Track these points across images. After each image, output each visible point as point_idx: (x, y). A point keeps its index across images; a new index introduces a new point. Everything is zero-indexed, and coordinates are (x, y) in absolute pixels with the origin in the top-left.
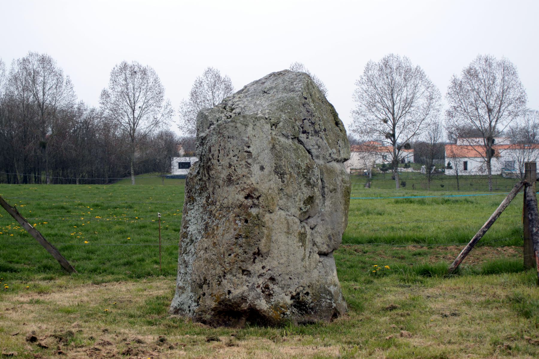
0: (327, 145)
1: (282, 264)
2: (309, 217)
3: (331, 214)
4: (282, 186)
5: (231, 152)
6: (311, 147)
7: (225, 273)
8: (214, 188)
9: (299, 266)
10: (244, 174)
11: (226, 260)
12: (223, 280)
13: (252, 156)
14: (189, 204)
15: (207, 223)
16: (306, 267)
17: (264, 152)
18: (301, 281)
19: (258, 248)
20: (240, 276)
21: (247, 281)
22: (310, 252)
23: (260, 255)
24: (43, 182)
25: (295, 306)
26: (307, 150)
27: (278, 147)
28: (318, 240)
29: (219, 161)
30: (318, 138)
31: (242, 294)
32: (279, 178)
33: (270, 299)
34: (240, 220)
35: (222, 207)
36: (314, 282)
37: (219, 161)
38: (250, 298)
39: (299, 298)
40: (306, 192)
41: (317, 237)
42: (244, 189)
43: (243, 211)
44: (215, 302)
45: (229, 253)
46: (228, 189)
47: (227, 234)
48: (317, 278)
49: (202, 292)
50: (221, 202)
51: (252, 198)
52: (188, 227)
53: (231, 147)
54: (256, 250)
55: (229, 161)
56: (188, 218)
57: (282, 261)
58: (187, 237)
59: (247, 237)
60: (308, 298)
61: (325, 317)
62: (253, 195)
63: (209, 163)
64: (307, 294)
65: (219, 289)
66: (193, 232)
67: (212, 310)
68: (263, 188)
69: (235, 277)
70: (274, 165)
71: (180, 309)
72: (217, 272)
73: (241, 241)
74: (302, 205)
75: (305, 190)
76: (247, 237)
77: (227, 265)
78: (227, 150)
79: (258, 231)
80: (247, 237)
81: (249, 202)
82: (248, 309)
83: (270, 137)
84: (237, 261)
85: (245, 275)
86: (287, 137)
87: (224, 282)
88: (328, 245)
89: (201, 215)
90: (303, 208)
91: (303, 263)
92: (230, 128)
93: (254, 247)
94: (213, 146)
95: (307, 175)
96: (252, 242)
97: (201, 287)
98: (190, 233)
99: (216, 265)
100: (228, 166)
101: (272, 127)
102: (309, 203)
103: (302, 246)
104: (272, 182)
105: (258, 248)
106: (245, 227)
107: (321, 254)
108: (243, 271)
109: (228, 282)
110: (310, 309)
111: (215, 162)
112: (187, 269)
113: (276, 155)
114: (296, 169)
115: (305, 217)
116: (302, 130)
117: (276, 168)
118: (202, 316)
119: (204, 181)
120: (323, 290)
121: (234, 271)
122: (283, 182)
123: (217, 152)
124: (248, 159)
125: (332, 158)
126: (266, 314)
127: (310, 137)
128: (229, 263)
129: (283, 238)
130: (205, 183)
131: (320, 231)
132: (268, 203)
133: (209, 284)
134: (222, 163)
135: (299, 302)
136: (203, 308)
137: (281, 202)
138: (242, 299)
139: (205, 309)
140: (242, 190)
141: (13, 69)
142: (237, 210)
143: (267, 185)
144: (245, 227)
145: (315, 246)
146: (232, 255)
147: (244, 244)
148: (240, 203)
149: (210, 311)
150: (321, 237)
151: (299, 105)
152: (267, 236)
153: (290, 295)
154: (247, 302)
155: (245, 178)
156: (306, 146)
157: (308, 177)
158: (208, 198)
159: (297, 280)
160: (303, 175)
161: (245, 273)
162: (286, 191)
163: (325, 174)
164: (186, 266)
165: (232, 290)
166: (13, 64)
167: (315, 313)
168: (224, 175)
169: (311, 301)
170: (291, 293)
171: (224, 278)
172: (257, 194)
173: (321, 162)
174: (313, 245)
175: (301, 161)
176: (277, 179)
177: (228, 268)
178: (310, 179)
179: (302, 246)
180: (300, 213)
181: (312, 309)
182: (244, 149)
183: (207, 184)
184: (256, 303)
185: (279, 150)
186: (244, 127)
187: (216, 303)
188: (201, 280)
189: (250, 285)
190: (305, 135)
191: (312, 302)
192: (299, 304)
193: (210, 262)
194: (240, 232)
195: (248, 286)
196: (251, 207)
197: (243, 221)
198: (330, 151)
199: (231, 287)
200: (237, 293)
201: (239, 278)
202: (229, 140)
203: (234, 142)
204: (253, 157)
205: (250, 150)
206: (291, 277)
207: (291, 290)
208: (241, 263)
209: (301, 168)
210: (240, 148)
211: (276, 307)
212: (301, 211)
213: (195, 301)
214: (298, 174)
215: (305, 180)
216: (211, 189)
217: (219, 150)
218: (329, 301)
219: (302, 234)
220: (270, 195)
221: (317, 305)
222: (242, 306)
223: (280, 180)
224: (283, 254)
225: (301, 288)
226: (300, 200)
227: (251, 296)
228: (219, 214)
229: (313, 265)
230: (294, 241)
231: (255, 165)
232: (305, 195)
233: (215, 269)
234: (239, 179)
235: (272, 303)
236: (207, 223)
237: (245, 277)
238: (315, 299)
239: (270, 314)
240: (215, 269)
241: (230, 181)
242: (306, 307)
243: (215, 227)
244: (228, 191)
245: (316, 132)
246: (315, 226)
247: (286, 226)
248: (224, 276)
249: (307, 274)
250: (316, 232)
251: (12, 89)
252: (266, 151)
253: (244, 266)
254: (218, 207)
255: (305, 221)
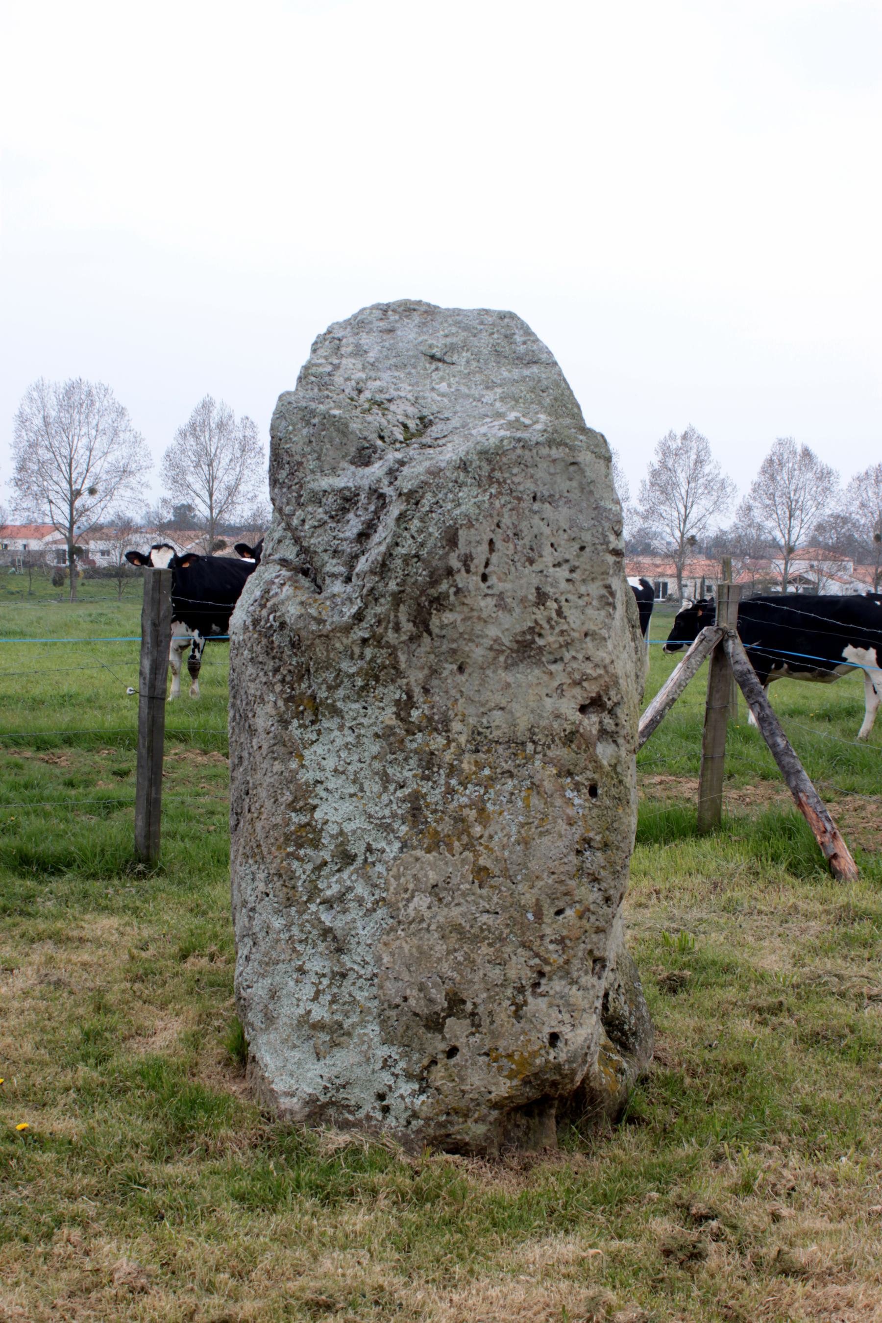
5: (547, 550)
7: (541, 974)
8: (434, 672)
10: (591, 626)
11: (548, 931)
12: (530, 999)
14: (295, 723)
15: (415, 798)
24: (821, 754)
29: (484, 578)
34: (577, 787)
35: (479, 741)
37: (484, 578)
42: (586, 678)
44: (510, 1077)
45: (561, 904)
46: (511, 679)
47: (546, 840)
49: (443, 1046)
50: (472, 721)
52: (315, 807)
53: (547, 531)
55: (535, 581)
56: (306, 776)
58: (316, 844)
59: (606, 845)
63: (444, 586)
65: (524, 1032)
66: (348, 827)
67: (495, 1106)
69: (575, 988)
71: (331, 1103)
72: (512, 974)
76: (606, 846)
77: (552, 947)
78: (526, 541)
81: (591, 723)
87: (536, 1005)
89: (377, 765)
92: (543, 465)
94: (470, 525)
97: (435, 1024)
98: (333, 829)
99: (508, 949)
100: (532, 597)
106: (595, 810)
109: (550, 1005)
111: (470, 581)
112: (345, 958)
118: (452, 1130)
119: (388, 645)
123: (485, 547)
128: (561, 941)
130: (393, 654)
133: (473, 1014)
134: (500, 586)
136: (452, 1101)
139: (463, 1104)
140: (577, 683)
142: (557, 752)
146: (569, 912)
148: (569, 728)
149: (484, 1110)
155: (589, 643)
158: (405, 705)
164: (339, 950)
165: (565, 1031)
168: (504, 627)
171: (534, 993)
177: (557, 959)
182: (608, 543)
183: (402, 658)
187: (516, 1082)
188: (431, 1001)
193: (476, 940)
199: (562, 1022)
201: (586, 989)
202: (536, 506)
203: (562, 514)
208: (595, 938)
210: (587, 537)
213: (409, 1076)
216: (415, 677)
217: (491, 542)
228: (480, 766)
233: (503, 963)
234: (567, 645)
236: (415, 798)
240: (503, 963)
241: (526, 649)
243: (472, 814)
244: (508, 685)
248: (536, 985)
254: (463, 739)
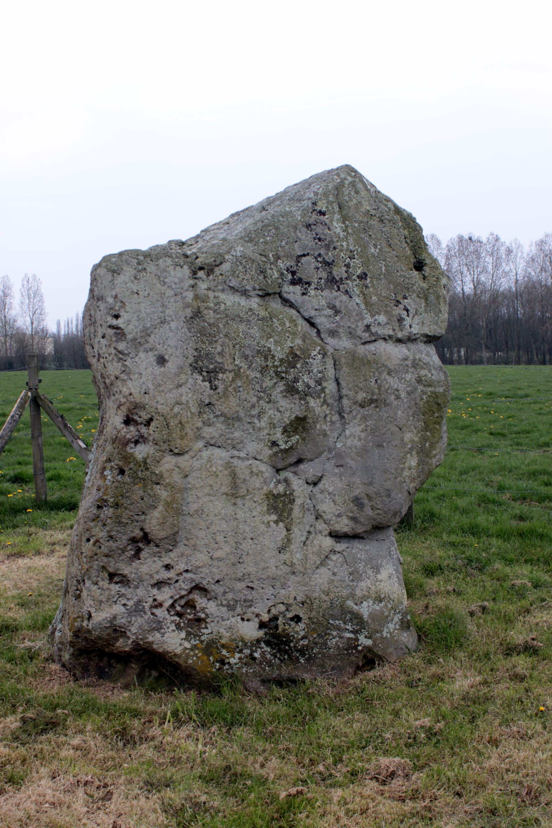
0: (363, 306)
1: (219, 559)
2: (300, 461)
3: (363, 452)
4: (210, 396)
6: (313, 313)
9: (272, 563)
13: (124, 335)
16: (292, 565)
17: (166, 326)
18: (283, 591)
19: (142, 529)
20: (105, 584)
21: (121, 596)
22: (309, 532)
23: (152, 544)
25: (268, 643)
26: (305, 319)
27: (210, 316)
28: (327, 507)
30: (335, 294)
31: (110, 622)
32: (204, 381)
33: (199, 629)
36: (316, 595)
38: (134, 629)
39: (277, 627)
40: (289, 409)
41: (322, 501)
43: (116, 451)
48: (325, 587)
51: (136, 423)
54: (138, 533)
57: (218, 554)
60: (297, 629)
61: (333, 669)
62: (136, 417)
64: (297, 619)
68: (161, 402)
70: (191, 352)
73: (108, 512)
74: (278, 436)
75: (284, 403)
76: (117, 505)
79: (141, 493)
80: (117, 505)
81: (131, 432)
82: (134, 649)
83: (190, 295)
84: (96, 554)
85: (117, 583)
86: (245, 293)
88: (354, 519)
90: (280, 443)
91: (285, 557)
93: (130, 528)
95: (286, 372)
96: (125, 515)
101: (195, 273)
102: (296, 431)
103: (276, 522)
104: (183, 390)
105: (142, 529)
107: (336, 536)
108: (112, 576)
110: (298, 651)
113: (202, 332)
114: (259, 361)
115: (287, 460)
116: (290, 277)
117: (197, 359)
120: (336, 612)
121: (94, 573)
122: (214, 388)
124: (117, 341)
125: (372, 334)
126: (181, 662)
127: (312, 292)
129: (219, 506)
131: (331, 490)
132: (170, 434)
135: (276, 636)
137: (208, 432)
138: (115, 630)
141: (531, 251)
143: (171, 397)
144: (116, 484)
145: (320, 521)
147: (109, 521)
150: (334, 502)
151: (295, 228)
152: (168, 505)
153: (257, 620)
154: (129, 638)
156: (301, 310)
157: (291, 377)
159: (272, 591)
160: (277, 373)
161: (116, 579)
162: (220, 407)
163: (345, 369)
166: (530, 246)
167: (308, 660)
169: (302, 633)
170: (257, 615)
172: (145, 416)
173: (344, 343)
174: (317, 518)
175: (276, 342)
176: (199, 382)
178: (296, 380)
179: (276, 522)
180: (270, 452)
181: (302, 652)
184: (150, 639)
185: (212, 321)
186: (109, 276)
189: (130, 603)
190: (298, 289)
191: (304, 638)
192: (275, 636)
194: (105, 494)
195: (124, 605)
196: (136, 442)
197: (116, 472)
198: (368, 320)
200: (100, 619)
201: (103, 589)
204: (129, 337)
205: (120, 322)
206: (250, 585)
207: (256, 611)
208: (105, 559)
209: (273, 357)
211: (210, 647)
212: (275, 449)
214: (264, 370)
215: (281, 384)
218: (351, 635)
219: (276, 497)
220: (176, 416)
221: (316, 644)
222: (118, 644)
223: (207, 384)
224: (220, 538)
225: (282, 608)
226: (273, 426)
227: (136, 625)
229: (314, 559)
230: (254, 514)
231: (142, 355)
232: (287, 414)
235: (203, 638)
237: (115, 588)
238: (314, 630)
239: (190, 661)
242: (289, 646)
245: (333, 282)
246: (320, 479)
247: (227, 481)
249: (298, 579)
250: (322, 492)
251: (530, 270)
252: (173, 325)
253: (112, 564)
255: (292, 469)
